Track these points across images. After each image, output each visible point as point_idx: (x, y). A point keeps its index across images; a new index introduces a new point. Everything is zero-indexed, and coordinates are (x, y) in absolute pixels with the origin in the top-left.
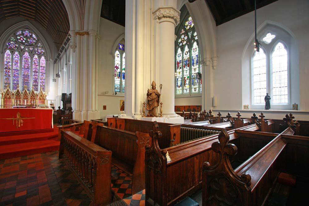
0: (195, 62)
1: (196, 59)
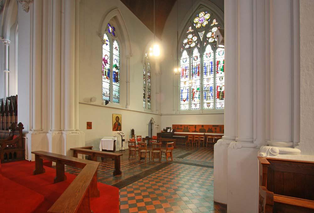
0: (208, 71)
1: (210, 67)
